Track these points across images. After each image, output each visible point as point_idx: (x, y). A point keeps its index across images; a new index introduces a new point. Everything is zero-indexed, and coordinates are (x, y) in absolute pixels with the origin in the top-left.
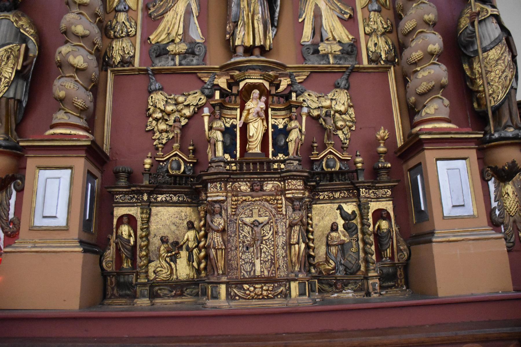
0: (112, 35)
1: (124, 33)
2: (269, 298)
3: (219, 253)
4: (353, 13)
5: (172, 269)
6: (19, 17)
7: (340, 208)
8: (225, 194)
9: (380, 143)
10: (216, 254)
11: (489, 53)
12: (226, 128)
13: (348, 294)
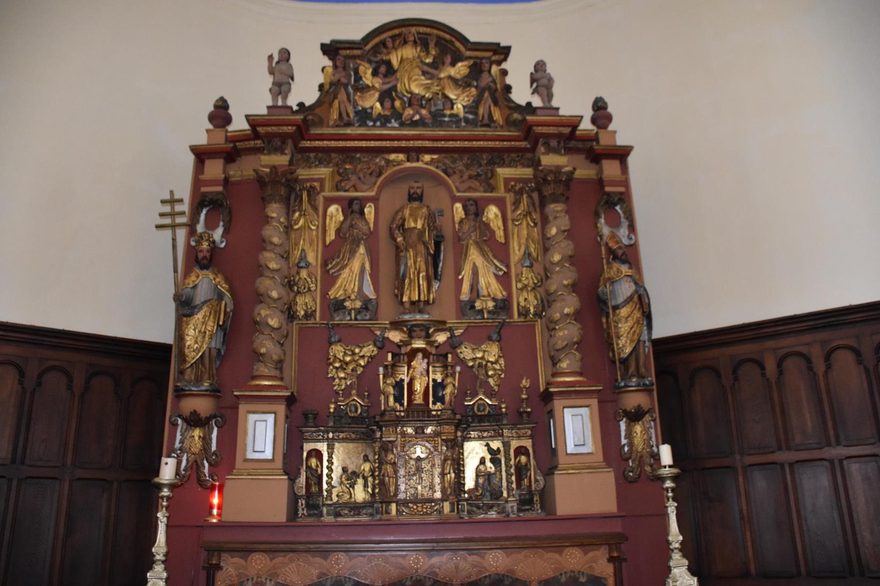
1: (306, 289)
2: (427, 514)
3: (391, 480)
6: (216, 275)
7: (487, 445)
9: (523, 391)
10: (389, 481)
12: (396, 382)
13: (493, 514)
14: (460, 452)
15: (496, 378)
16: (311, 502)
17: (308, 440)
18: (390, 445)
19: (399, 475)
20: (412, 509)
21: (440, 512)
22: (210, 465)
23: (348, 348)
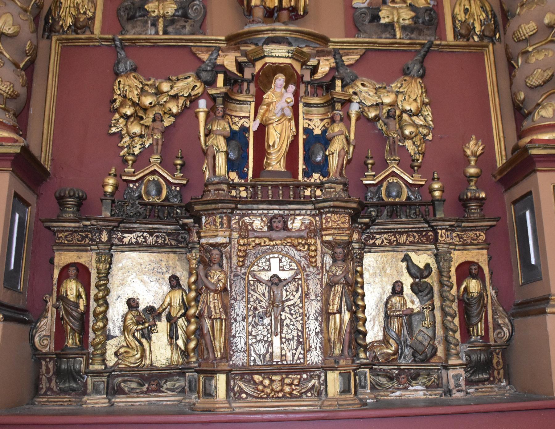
3: (217, 324)
5: (143, 351)
7: (407, 259)
10: (213, 326)
12: (233, 132)
14: (357, 271)
15: (417, 140)
16: (64, 366)
18: (215, 252)
19: (233, 314)
20: (260, 387)
21: (319, 393)
23: (149, 83)
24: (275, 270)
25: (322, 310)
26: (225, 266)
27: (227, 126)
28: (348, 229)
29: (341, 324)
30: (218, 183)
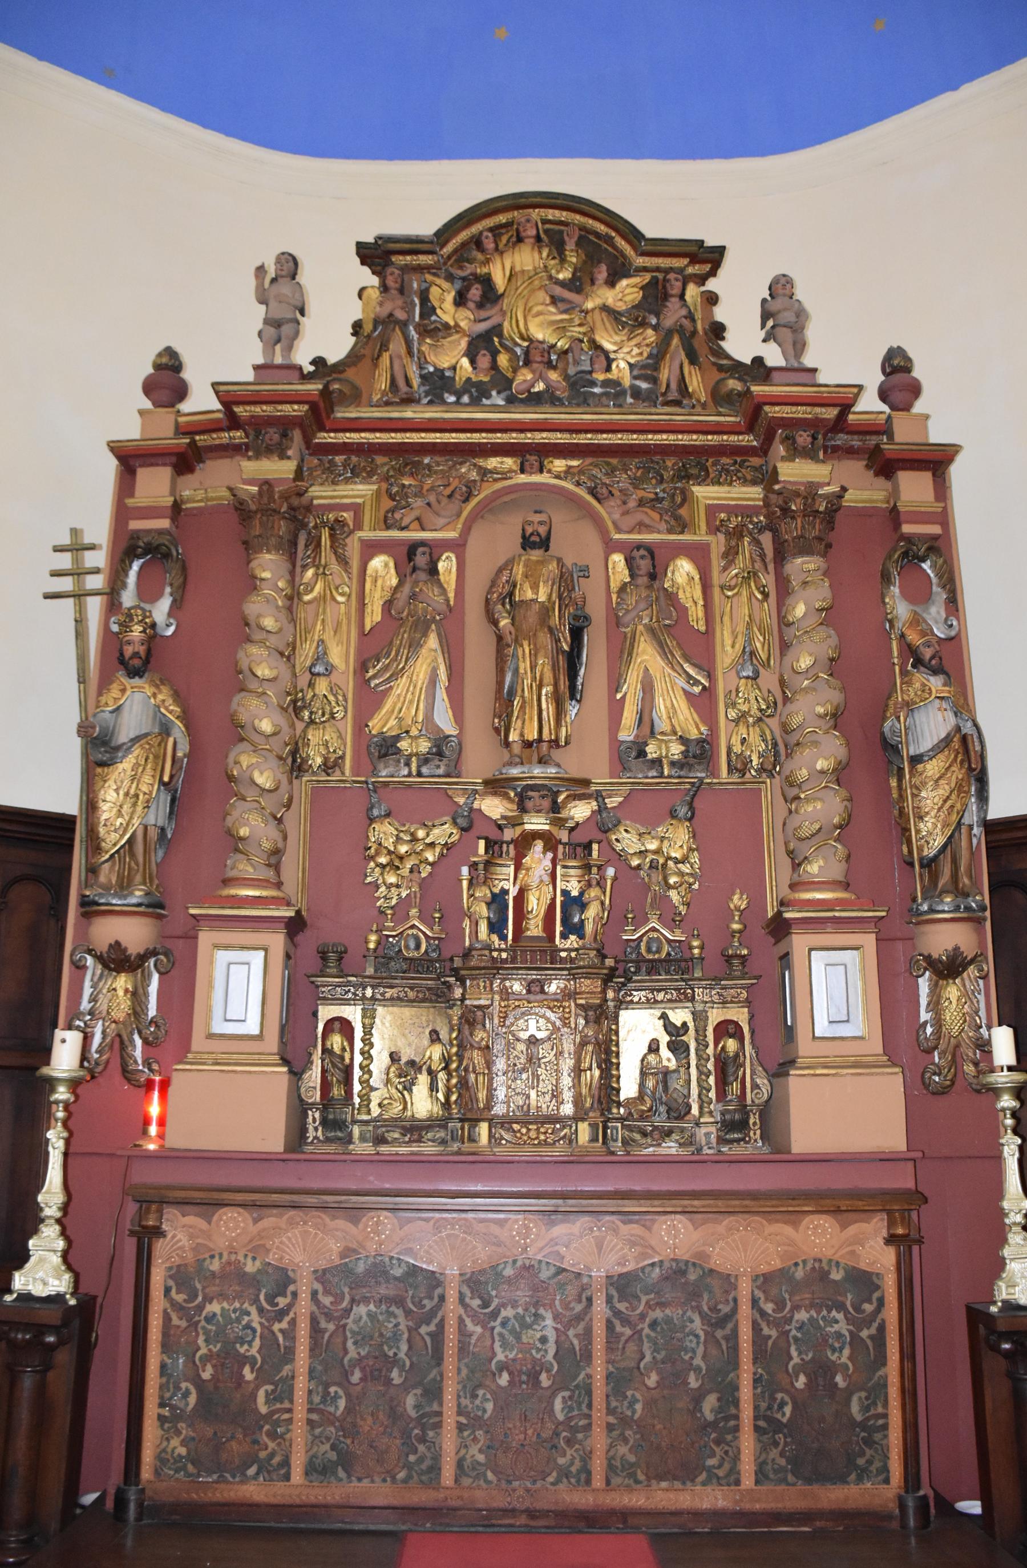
0: (306, 717)
3: (481, 1078)
4: (710, 682)
5: (405, 1103)
6: (157, 686)
7: (664, 1017)
8: (490, 996)
11: (928, 766)
12: (494, 895)
14: (611, 1029)
16: (331, 1117)
17: (327, 1001)
18: (479, 1013)
21: (571, 1141)
22: (146, 1042)
23: (403, 829)
24: (532, 1030)
25: (574, 1067)
26: (487, 1026)
27: (488, 892)
28: (600, 993)
29: (591, 1080)
30: (481, 949)
